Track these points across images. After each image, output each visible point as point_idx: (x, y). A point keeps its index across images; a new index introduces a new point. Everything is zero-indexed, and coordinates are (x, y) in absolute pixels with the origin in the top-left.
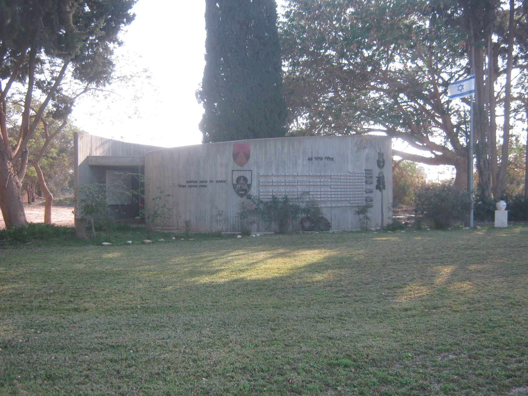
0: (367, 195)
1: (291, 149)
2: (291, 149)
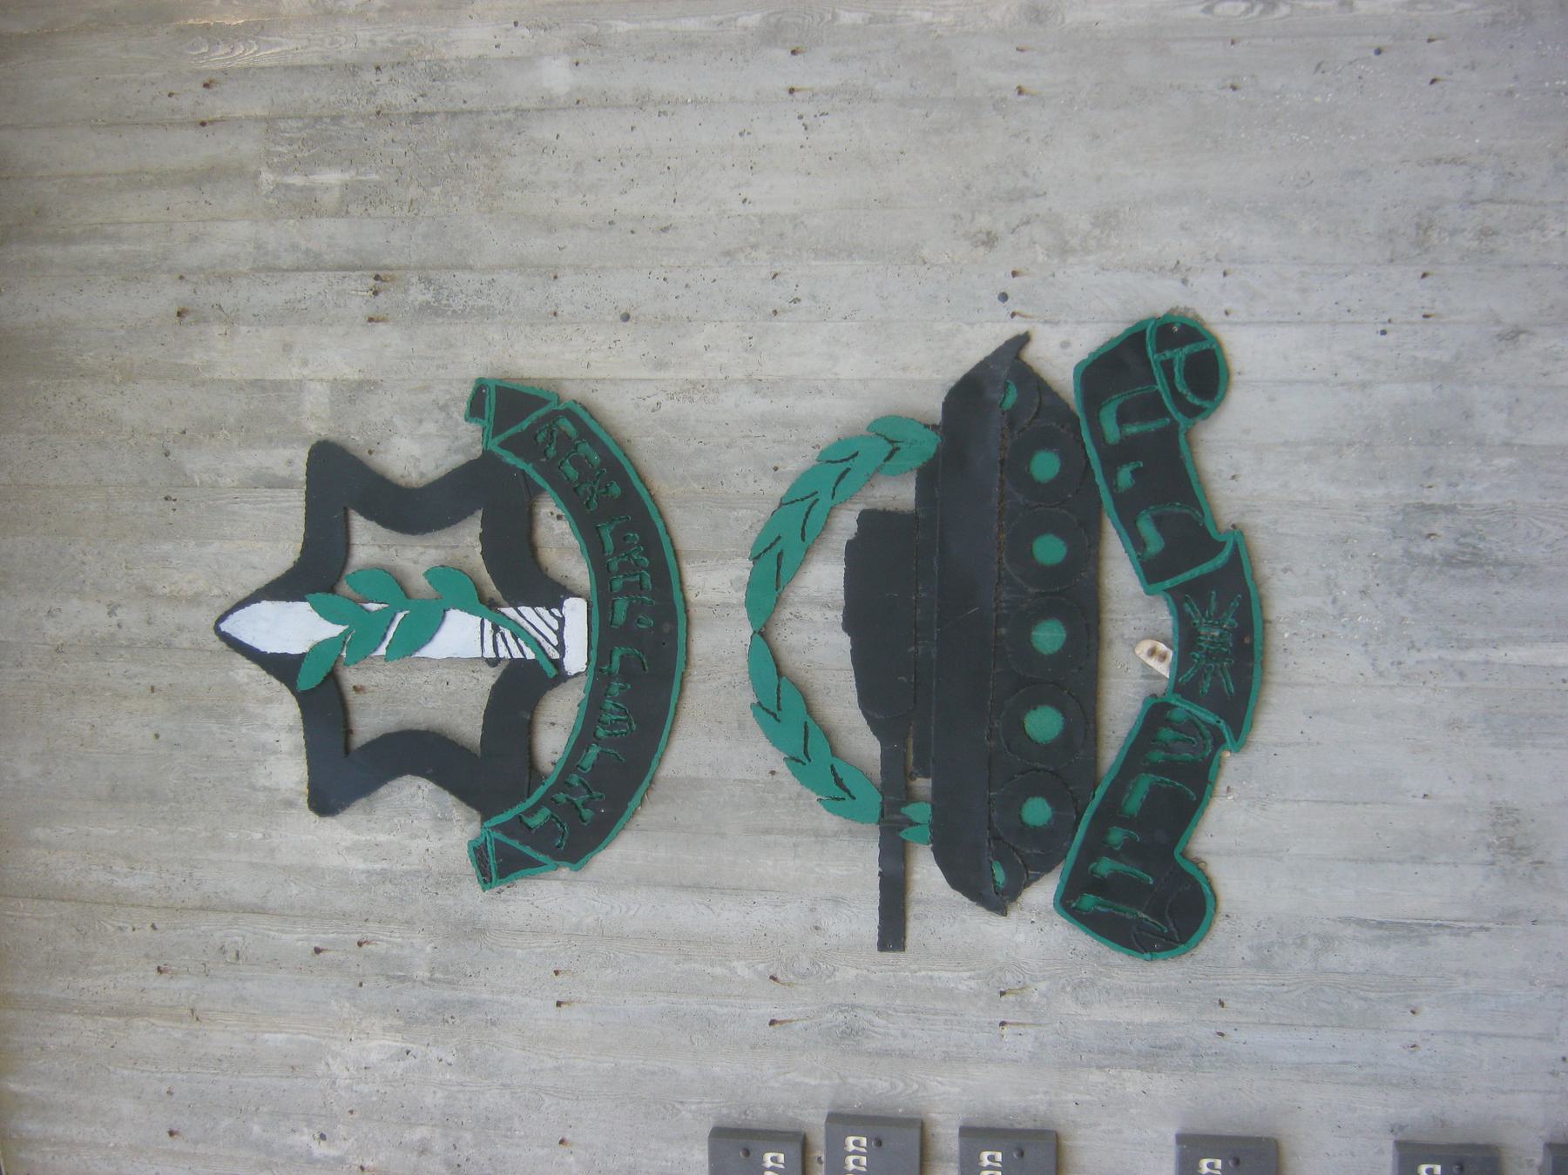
1: (106, 250)
2: (106, 250)
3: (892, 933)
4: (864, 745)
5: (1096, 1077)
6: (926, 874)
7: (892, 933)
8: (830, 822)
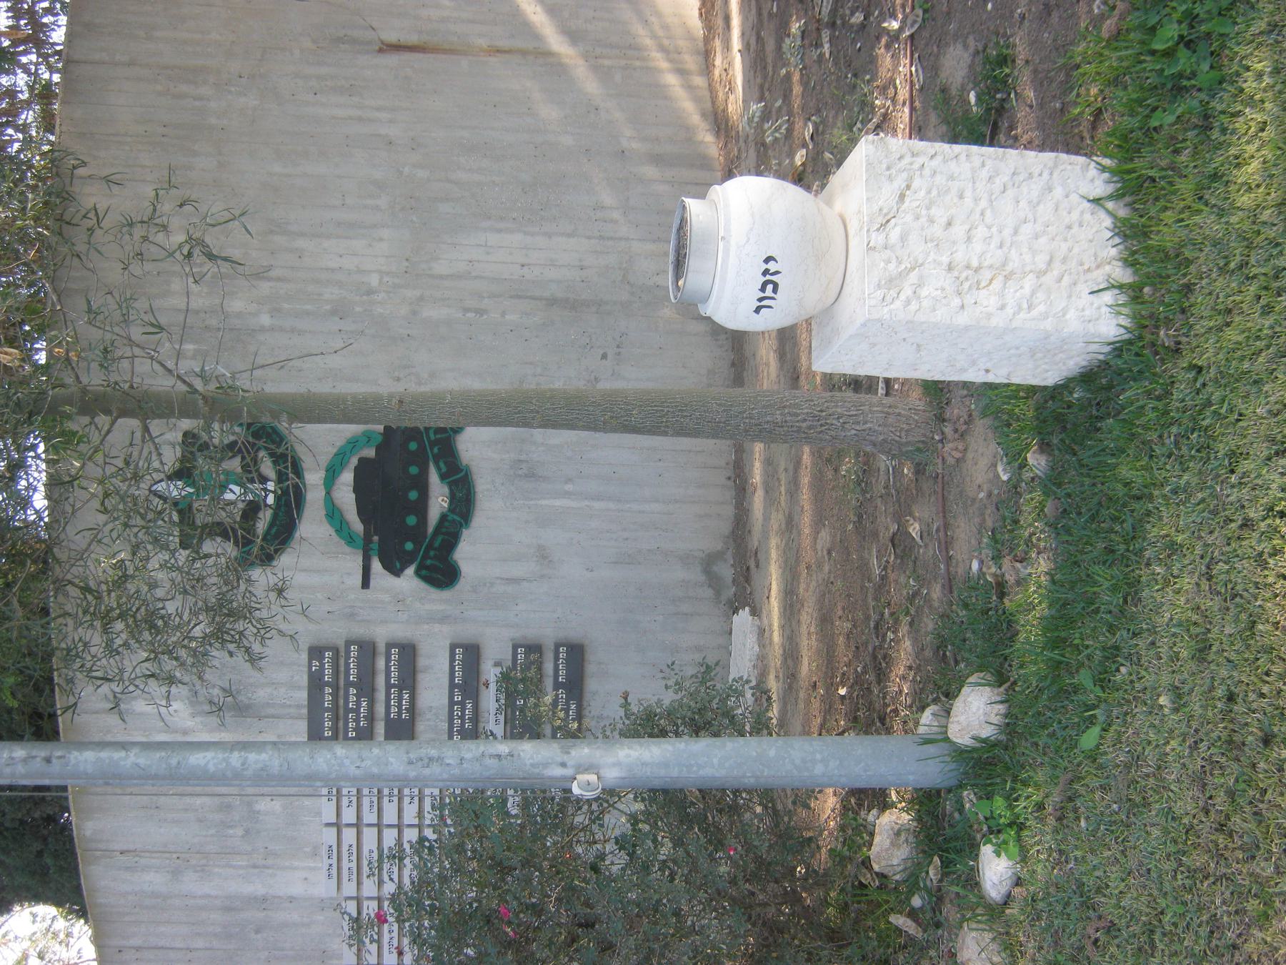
0: (493, 721)
3: (366, 583)
4: (358, 526)
5: (426, 627)
6: (376, 565)
7: (366, 583)
8: (347, 549)
